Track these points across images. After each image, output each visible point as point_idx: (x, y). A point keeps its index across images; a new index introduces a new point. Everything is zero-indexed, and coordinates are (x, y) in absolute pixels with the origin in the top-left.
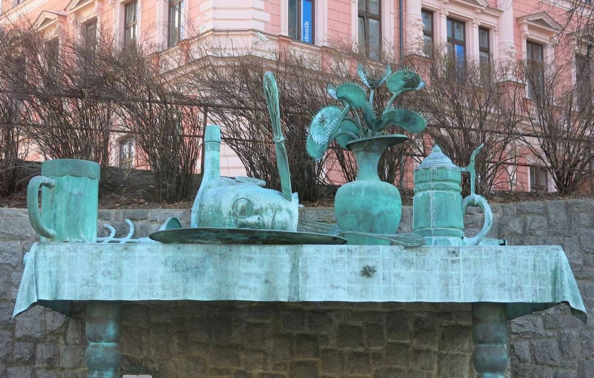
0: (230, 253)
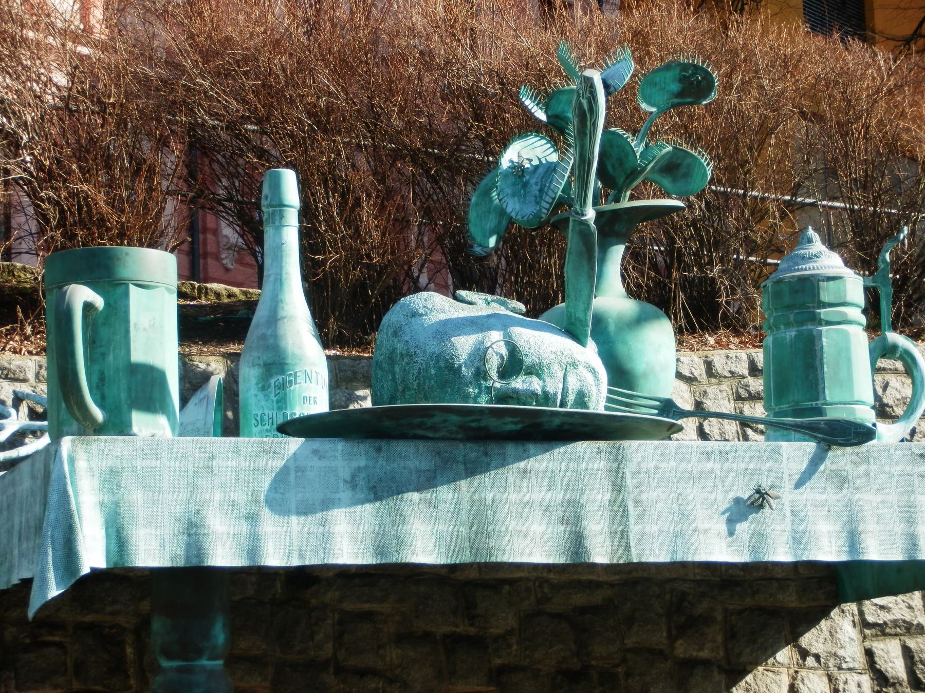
0: (485, 459)
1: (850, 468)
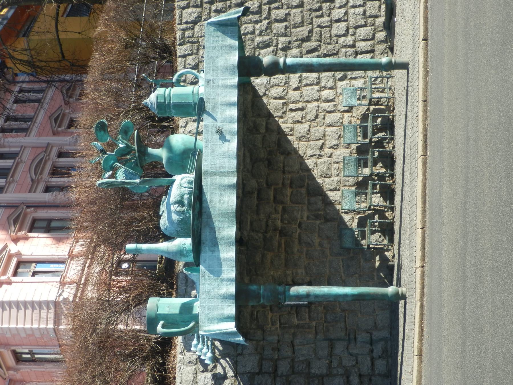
1: (211, 104)
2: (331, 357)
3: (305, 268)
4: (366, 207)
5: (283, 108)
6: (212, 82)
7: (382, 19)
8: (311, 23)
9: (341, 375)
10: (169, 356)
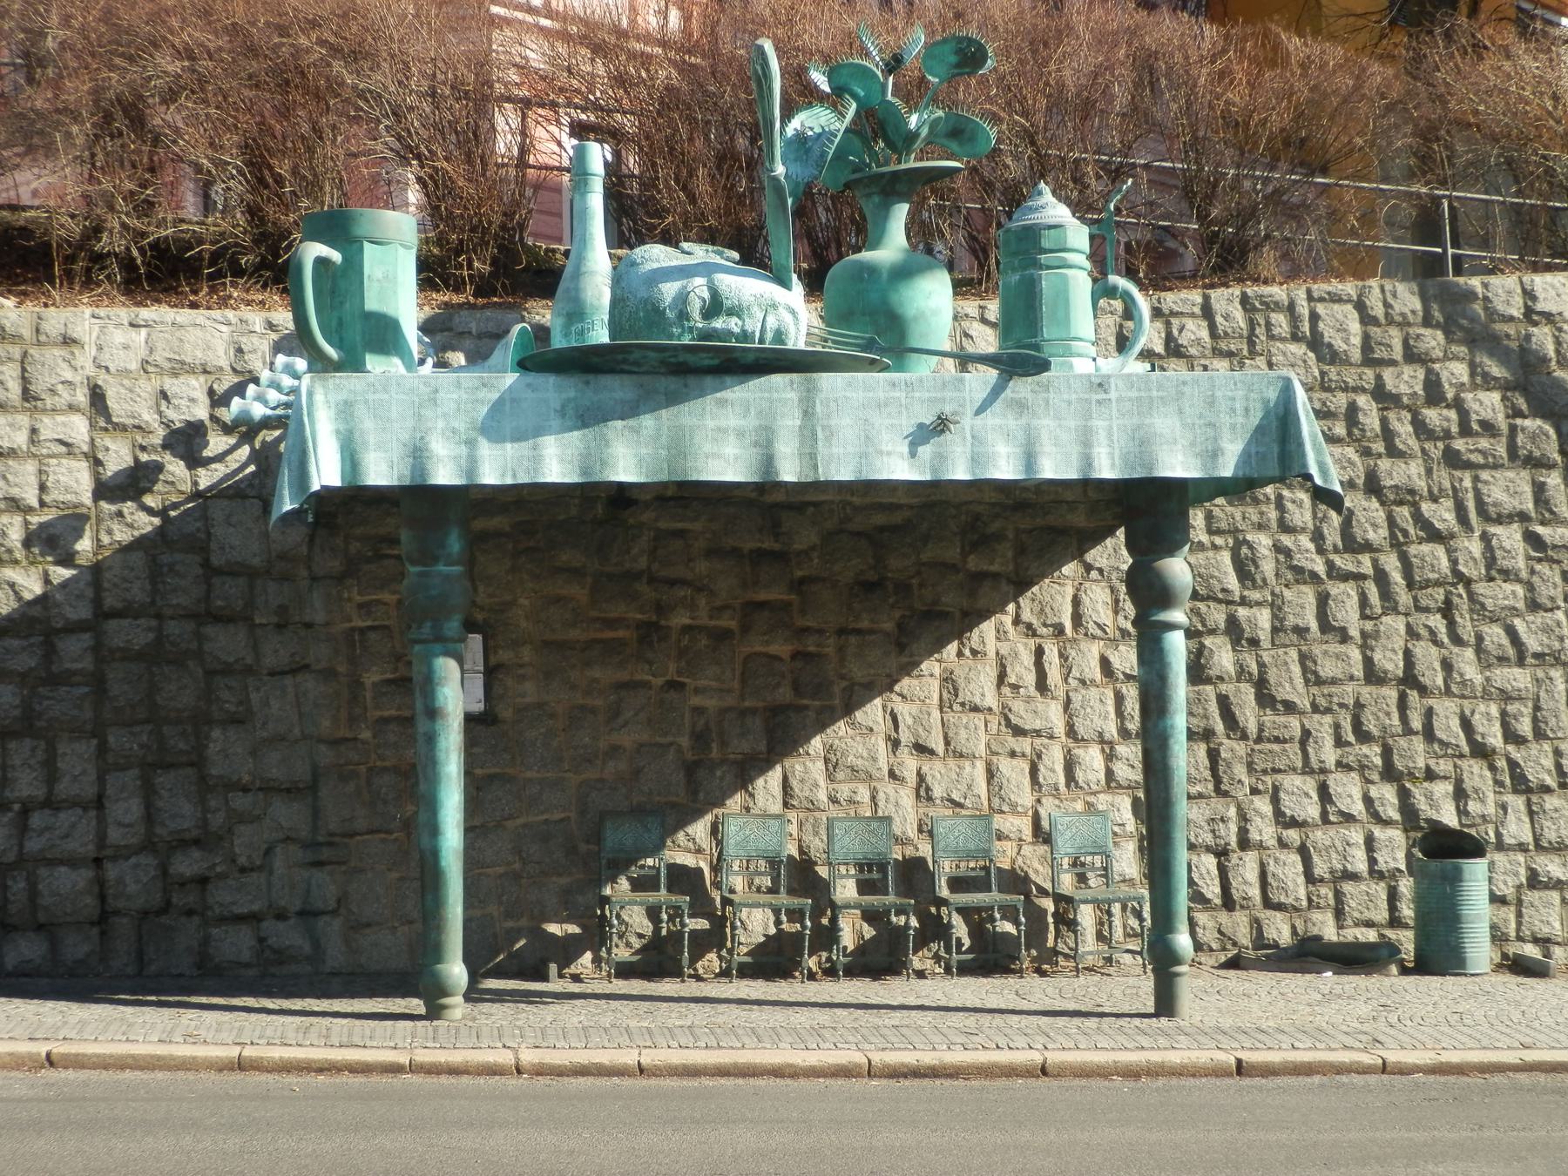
1: (1029, 396)
2: (260, 789)
3: (540, 705)
4: (732, 891)
5: (1045, 625)
6: (1102, 396)
7: (1330, 933)
8: (1315, 708)
9: (205, 820)
10: (264, 287)
